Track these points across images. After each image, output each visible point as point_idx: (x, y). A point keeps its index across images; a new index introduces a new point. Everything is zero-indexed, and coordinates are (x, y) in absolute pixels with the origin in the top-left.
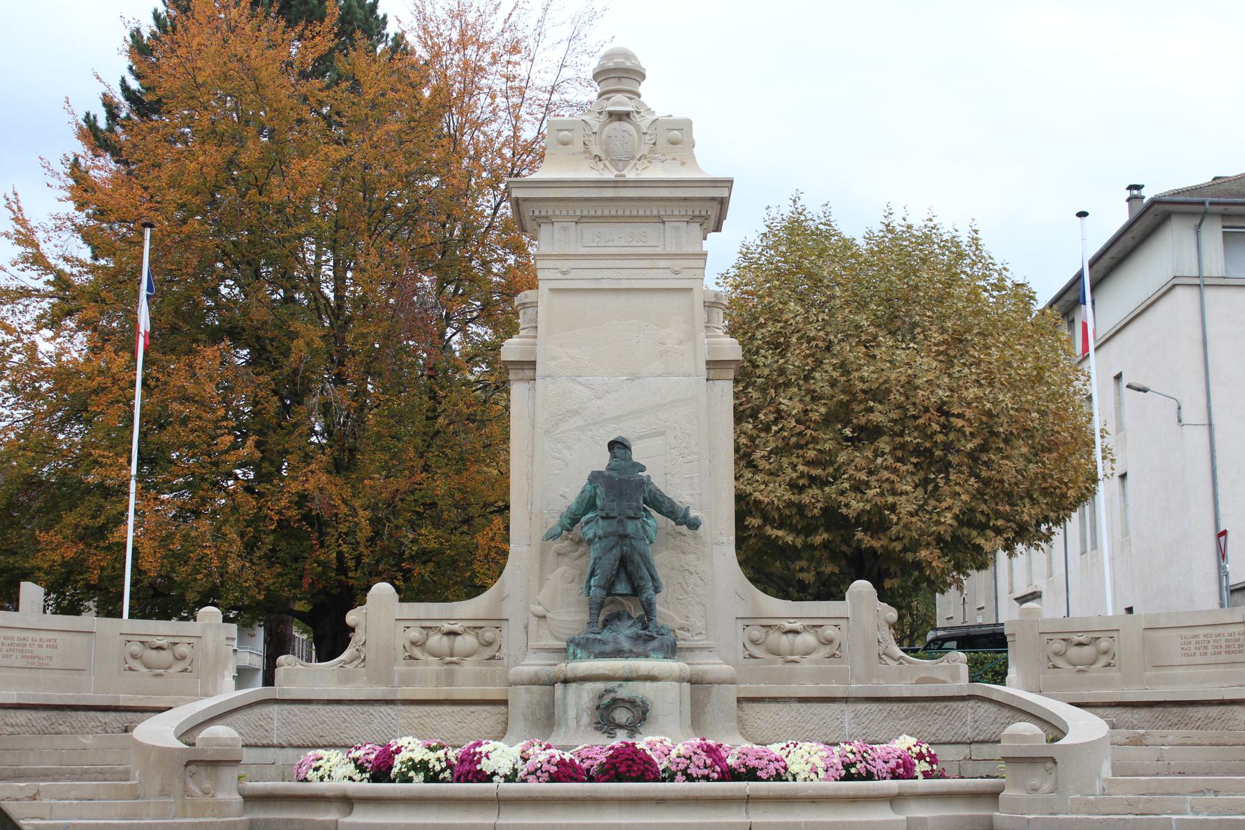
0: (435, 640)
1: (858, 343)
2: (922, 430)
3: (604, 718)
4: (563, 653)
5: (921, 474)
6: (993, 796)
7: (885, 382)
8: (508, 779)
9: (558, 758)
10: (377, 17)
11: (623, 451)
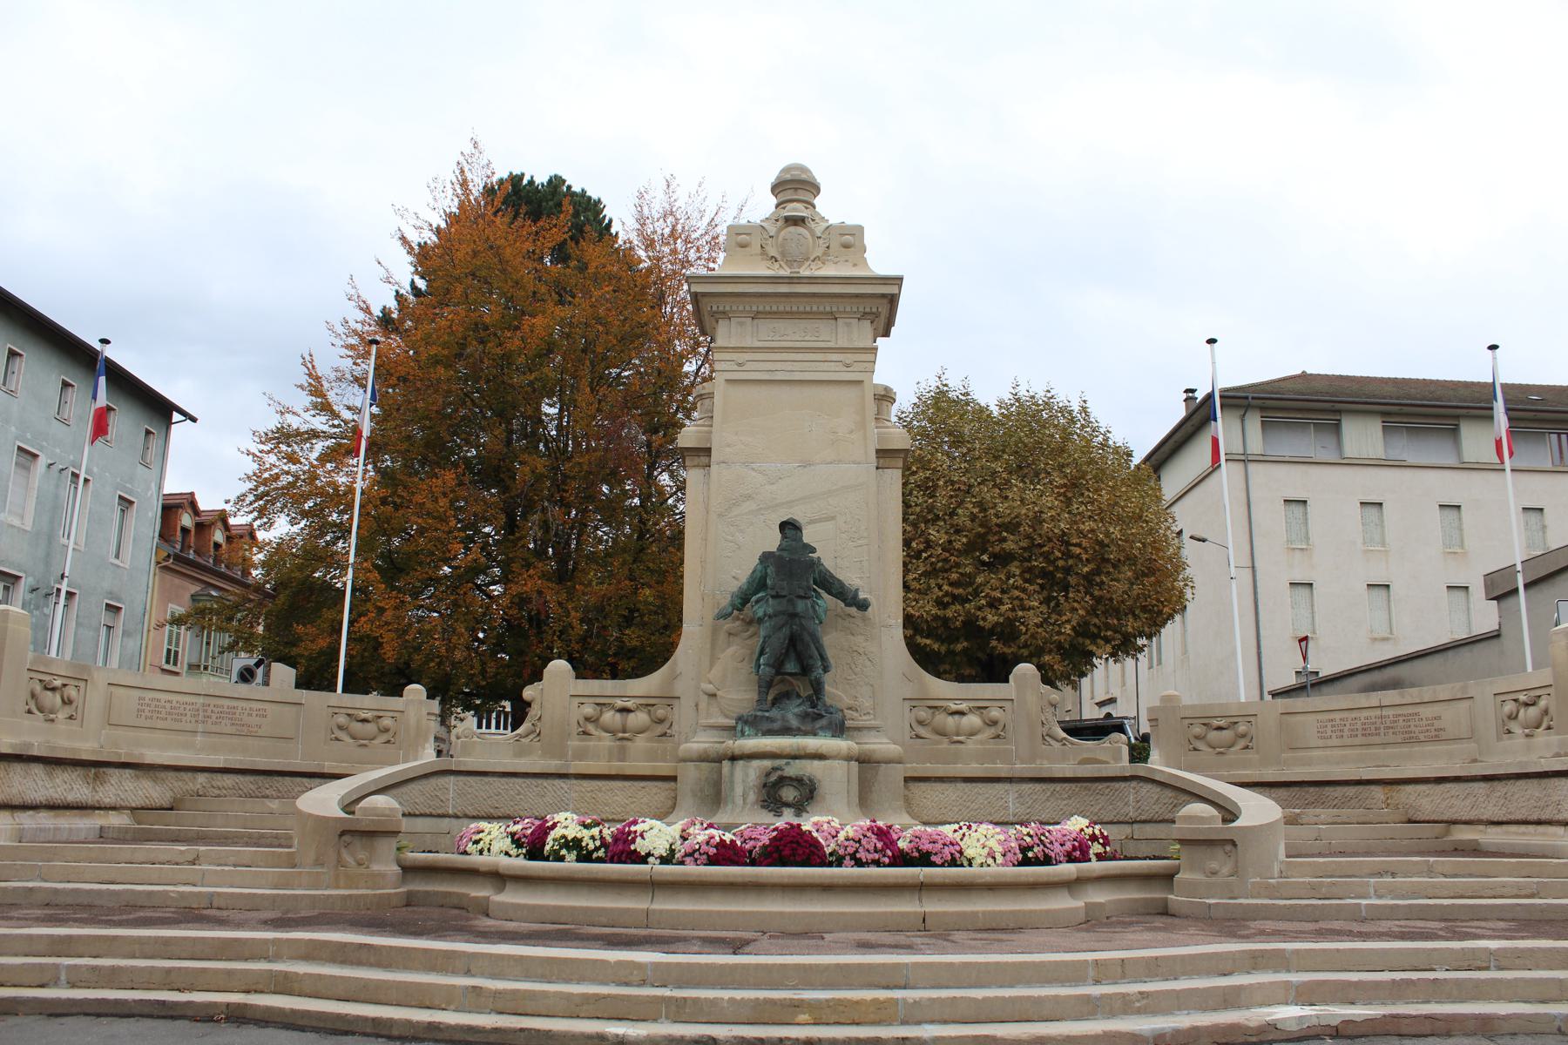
0: (609, 717)
1: (995, 486)
2: (1046, 556)
3: (771, 796)
4: (731, 730)
5: (1045, 593)
6: (1167, 878)
7: (1017, 517)
8: (665, 860)
9: (718, 839)
10: (611, 234)
11: (793, 532)
